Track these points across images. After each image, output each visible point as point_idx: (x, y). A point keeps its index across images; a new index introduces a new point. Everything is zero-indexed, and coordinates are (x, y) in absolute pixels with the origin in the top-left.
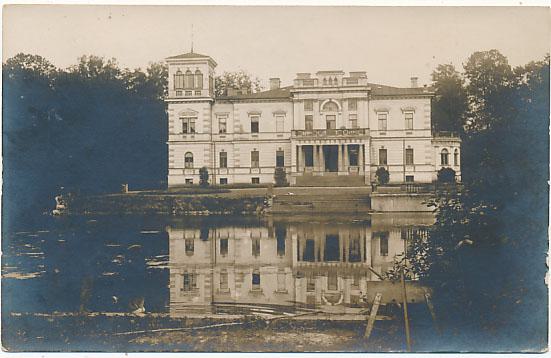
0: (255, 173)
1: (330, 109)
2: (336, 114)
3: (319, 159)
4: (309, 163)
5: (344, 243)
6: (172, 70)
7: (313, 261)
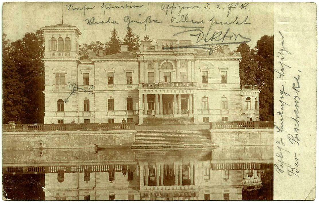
0: (111, 115)
1: (167, 68)
2: (171, 70)
3: (159, 105)
4: (152, 106)
5: (178, 147)
6: (47, 36)
7: (163, 95)
